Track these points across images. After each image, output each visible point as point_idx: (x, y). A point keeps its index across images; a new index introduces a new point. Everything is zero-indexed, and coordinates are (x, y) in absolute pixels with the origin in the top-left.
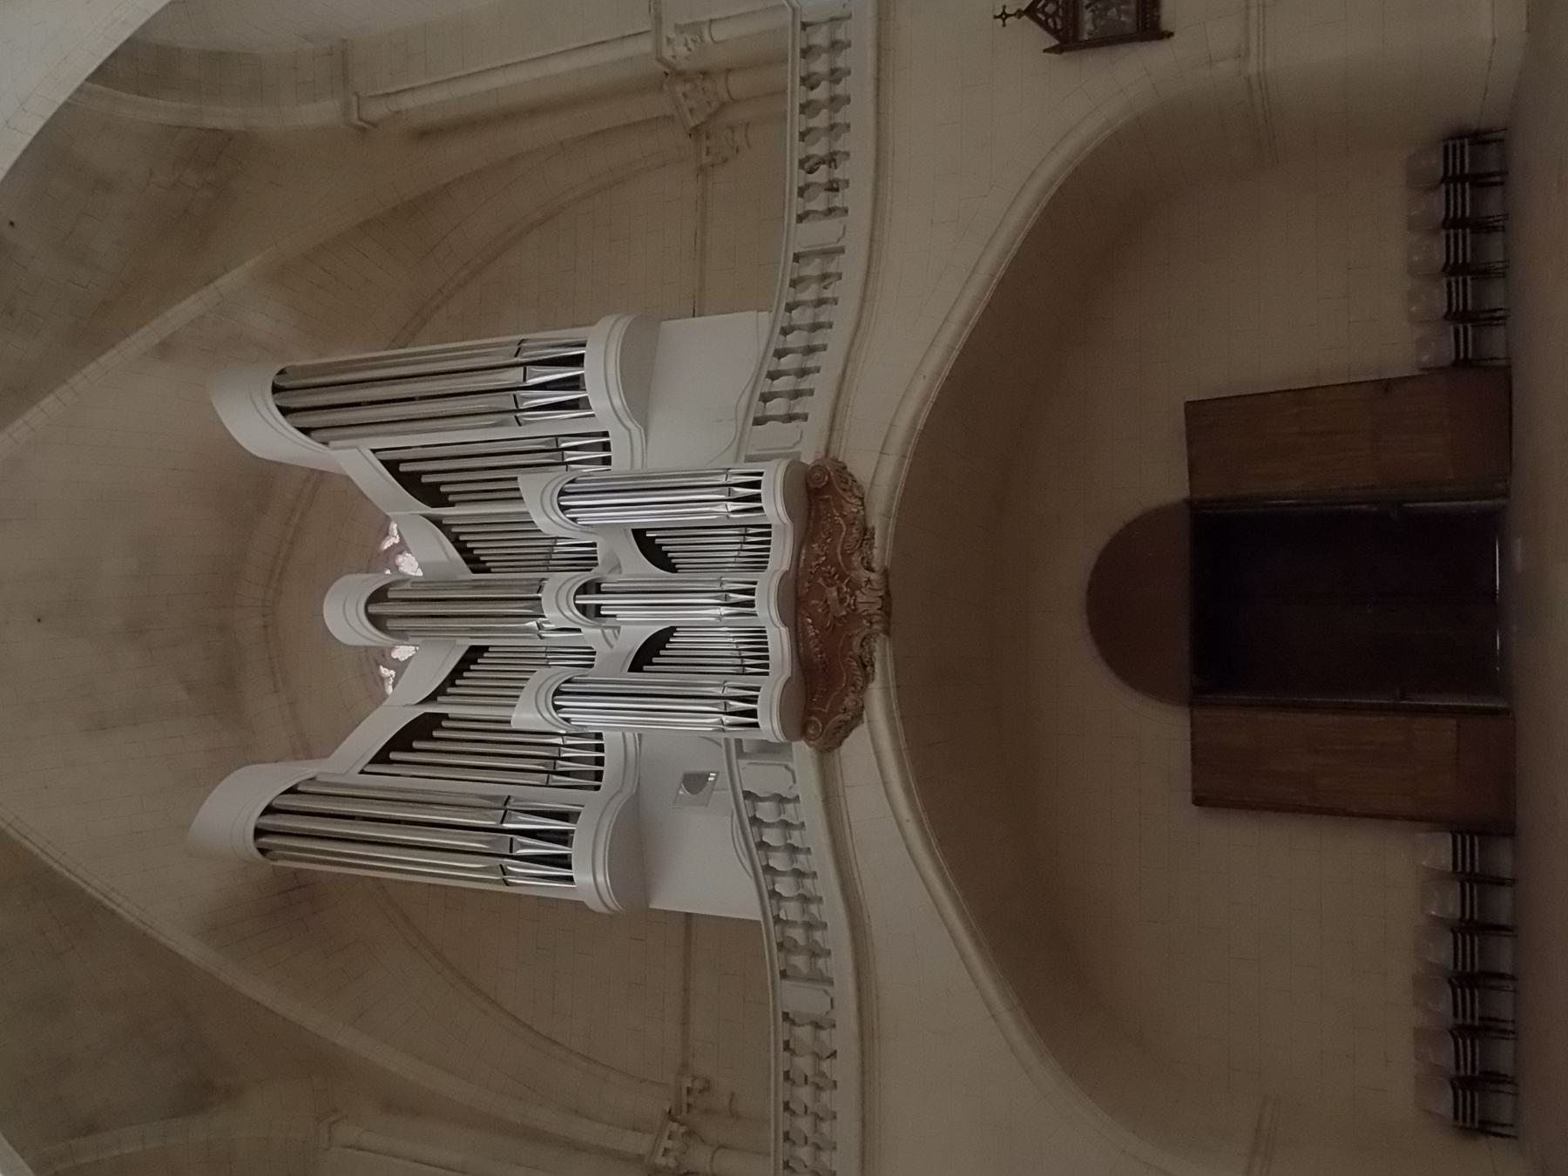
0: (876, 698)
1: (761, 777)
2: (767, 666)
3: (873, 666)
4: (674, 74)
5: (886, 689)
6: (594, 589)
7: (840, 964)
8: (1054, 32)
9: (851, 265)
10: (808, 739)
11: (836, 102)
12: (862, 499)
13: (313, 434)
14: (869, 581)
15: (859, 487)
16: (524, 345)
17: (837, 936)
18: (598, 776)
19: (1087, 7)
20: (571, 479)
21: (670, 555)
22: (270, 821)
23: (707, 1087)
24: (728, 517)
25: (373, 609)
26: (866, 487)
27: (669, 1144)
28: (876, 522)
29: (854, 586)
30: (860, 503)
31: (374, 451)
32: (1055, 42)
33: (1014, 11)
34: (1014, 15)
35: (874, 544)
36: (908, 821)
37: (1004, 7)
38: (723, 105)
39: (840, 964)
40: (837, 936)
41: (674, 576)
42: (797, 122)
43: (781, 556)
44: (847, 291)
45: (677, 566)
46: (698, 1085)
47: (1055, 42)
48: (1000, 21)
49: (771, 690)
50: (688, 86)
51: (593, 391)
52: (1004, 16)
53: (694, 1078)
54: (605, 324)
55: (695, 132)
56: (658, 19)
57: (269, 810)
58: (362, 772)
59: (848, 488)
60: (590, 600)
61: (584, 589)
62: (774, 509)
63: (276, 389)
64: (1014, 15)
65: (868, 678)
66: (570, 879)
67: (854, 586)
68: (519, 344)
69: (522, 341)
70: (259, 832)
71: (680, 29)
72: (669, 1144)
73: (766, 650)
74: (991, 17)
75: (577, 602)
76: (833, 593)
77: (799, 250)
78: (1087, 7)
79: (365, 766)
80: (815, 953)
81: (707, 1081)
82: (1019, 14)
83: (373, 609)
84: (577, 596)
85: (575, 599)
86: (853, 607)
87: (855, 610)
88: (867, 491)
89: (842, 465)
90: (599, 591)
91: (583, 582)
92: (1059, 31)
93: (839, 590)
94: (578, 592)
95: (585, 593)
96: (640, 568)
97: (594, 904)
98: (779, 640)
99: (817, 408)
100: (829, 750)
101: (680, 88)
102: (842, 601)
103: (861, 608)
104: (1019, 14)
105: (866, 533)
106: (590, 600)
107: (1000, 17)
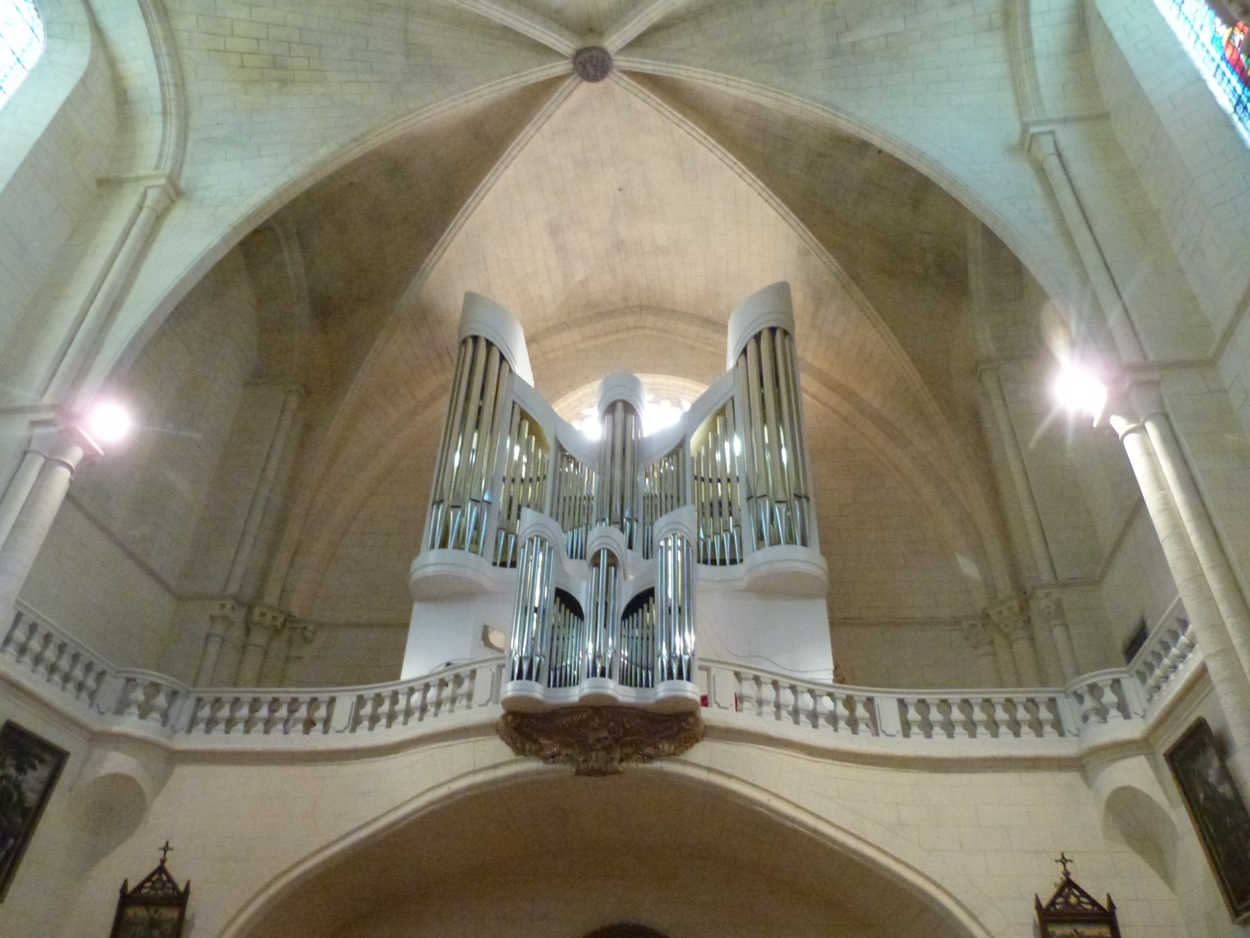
0: (531, 765)
1: (482, 686)
2: (555, 686)
3: (554, 763)
4: (1025, 598)
5: (538, 772)
6: (610, 561)
7: (365, 738)
8: (1053, 903)
9: (864, 742)
10: (504, 717)
11: (1015, 726)
12: (674, 754)
13: (743, 357)
14: (612, 760)
15: (682, 752)
16: (804, 501)
17: (383, 735)
18: (503, 564)
19: (1076, 931)
20: (691, 543)
21: (635, 615)
22: (483, 345)
23: (307, 641)
24: (659, 656)
25: (620, 406)
26: (683, 757)
27: (269, 616)
28: (657, 765)
29: (608, 749)
30: (670, 752)
31: (732, 399)
32: (1044, 903)
33: (1068, 869)
34: (1065, 869)
35: (640, 762)
36: (449, 788)
37: (1071, 861)
38: (1007, 636)
39: (365, 738)
40: (383, 735)
41: (620, 620)
42: (998, 696)
43: (624, 694)
44: (842, 739)
45: (627, 621)
46: (308, 634)
47: (1044, 903)
48: (1059, 858)
49: (537, 690)
50: (1016, 609)
51: (768, 552)
52: (1064, 861)
53: (314, 633)
54: (822, 562)
55: (986, 616)
56: (1064, 585)
57: (489, 344)
58: (514, 403)
59: (682, 743)
60: (603, 560)
61: (611, 555)
62: (662, 690)
63: (773, 330)
64: (1065, 869)
65: (545, 759)
66: (433, 546)
67: (608, 749)
68: (805, 496)
69: (807, 498)
70: (475, 339)
71: (1059, 604)
72: (269, 616)
73: (560, 686)
74: (1063, 851)
75: (602, 551)
76: (604, 734)
77: (877, 701)
78: (1076, 931)
79: (518, 405)
80: (374, 720)
81: (312, 641)
82: (1067, 874)
83: (620, 406)
84: (606, 551)
85: (604, 549)
86: (594, 748)
87: (592, 750)
88: (678, 757)
89: (700, 738)
90: (609, 565)
91: (616, 554)
92: (1055, 907)
93: (606, 738)
94: (608, 550)
95: (608, 555)
96: (625, 596)
97: (417, 562)
98: (574, 695)
99: (746, 720)
100: (498, 731)
101: (1015, 604)
102: (599, 740)
103: (593, 755)
104: (1067, 874)
105: (650, 758)
106: (603, 560)
107: (1063, 857)
